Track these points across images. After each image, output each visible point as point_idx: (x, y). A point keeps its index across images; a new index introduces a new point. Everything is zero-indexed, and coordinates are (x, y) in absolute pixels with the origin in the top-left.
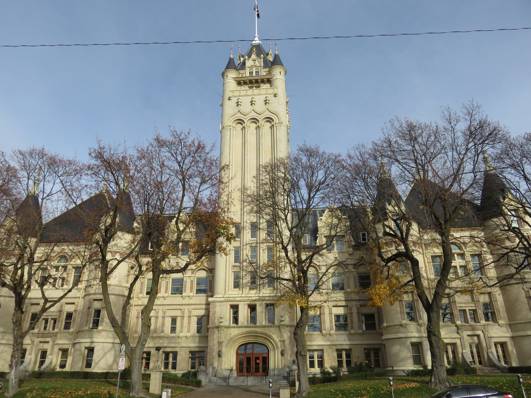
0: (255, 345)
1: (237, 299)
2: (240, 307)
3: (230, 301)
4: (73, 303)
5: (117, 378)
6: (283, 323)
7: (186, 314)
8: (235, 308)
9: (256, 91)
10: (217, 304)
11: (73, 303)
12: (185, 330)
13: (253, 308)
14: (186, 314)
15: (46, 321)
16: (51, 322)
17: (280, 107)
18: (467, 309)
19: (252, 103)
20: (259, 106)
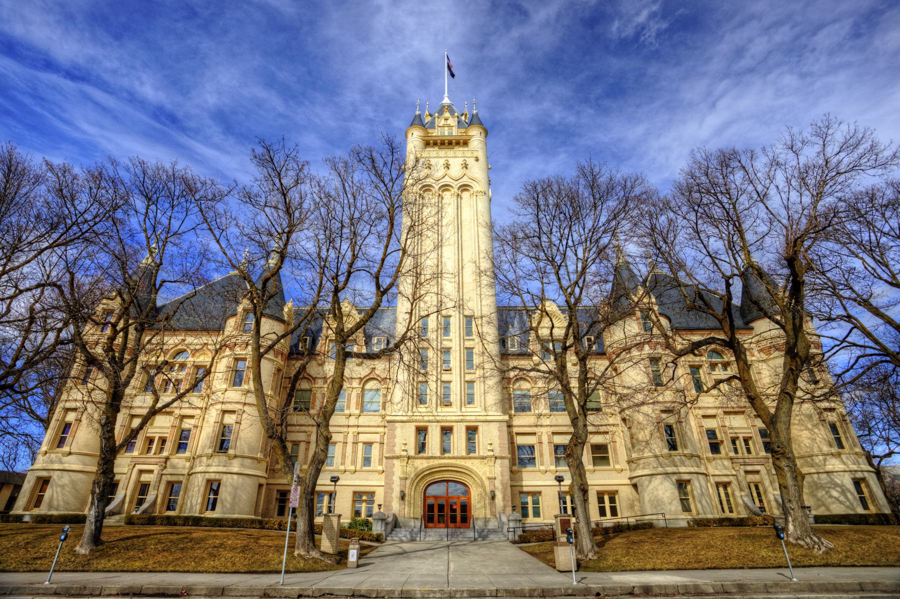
0: (450, 484)
1: (449, 418)
2: (430, 429)
3: (416, 421)
4: (534, 434)
5: (282, 554)
6: (588, 465)
7: (350, 439)
8: (421, 431)
9: (450, 153)
10: (397, 424)
11: (534, 434)
12: (348, 461)
13: (446, 431)
14: (350, 439)
15: (151, 441)
16: (296, 490)
17: (478, 171)
18: (741, 436)
19: (447, 166)
20: (456, 170)
